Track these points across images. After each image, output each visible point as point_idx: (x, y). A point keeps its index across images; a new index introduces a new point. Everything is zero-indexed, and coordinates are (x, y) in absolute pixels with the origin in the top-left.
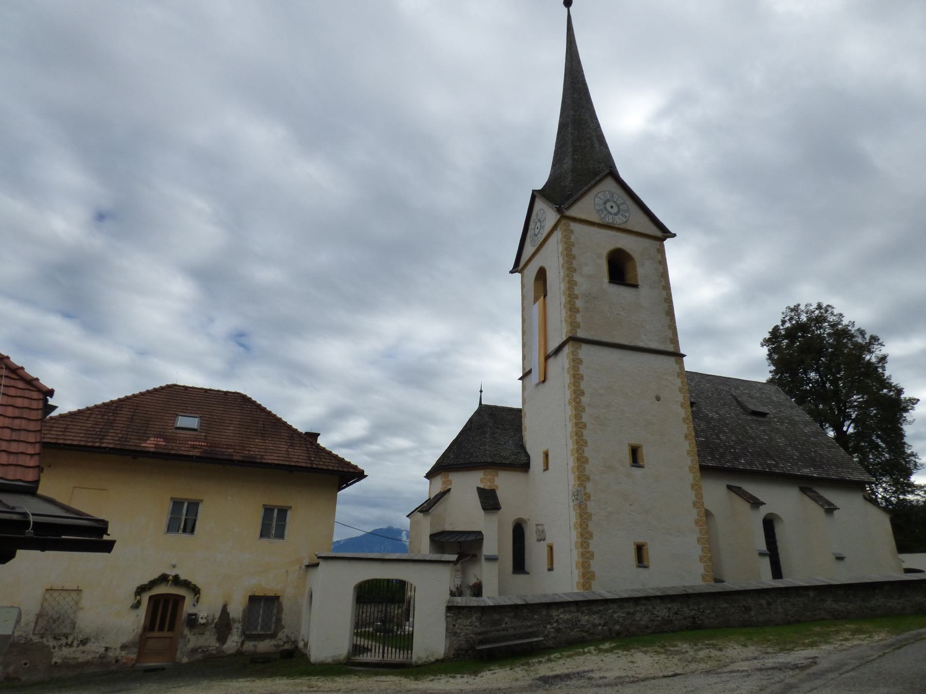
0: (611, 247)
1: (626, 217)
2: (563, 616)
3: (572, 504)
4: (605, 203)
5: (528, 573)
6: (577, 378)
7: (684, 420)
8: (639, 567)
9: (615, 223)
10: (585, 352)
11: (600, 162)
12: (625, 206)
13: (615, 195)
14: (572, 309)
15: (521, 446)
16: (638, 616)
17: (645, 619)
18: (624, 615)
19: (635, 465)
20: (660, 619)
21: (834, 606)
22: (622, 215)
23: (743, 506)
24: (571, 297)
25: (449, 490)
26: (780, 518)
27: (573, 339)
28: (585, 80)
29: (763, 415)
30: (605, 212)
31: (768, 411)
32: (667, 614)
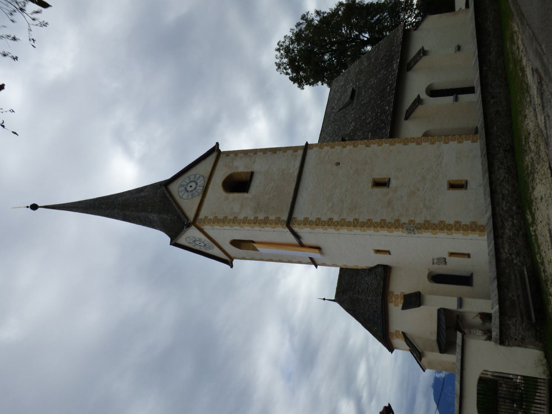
0: (221, 190)
1: (199, 177)
3: (417, 235)
4: (187, 191)
6: (318, 223)
8: (466, 188)
12: (191, 177)
13: (182, 184)
18: (504, 202)
19: (388, 184)
22: (198, 179)
23: (420, 110)
27: (289, 223)
29: (353, 92)
30: (194, 192)
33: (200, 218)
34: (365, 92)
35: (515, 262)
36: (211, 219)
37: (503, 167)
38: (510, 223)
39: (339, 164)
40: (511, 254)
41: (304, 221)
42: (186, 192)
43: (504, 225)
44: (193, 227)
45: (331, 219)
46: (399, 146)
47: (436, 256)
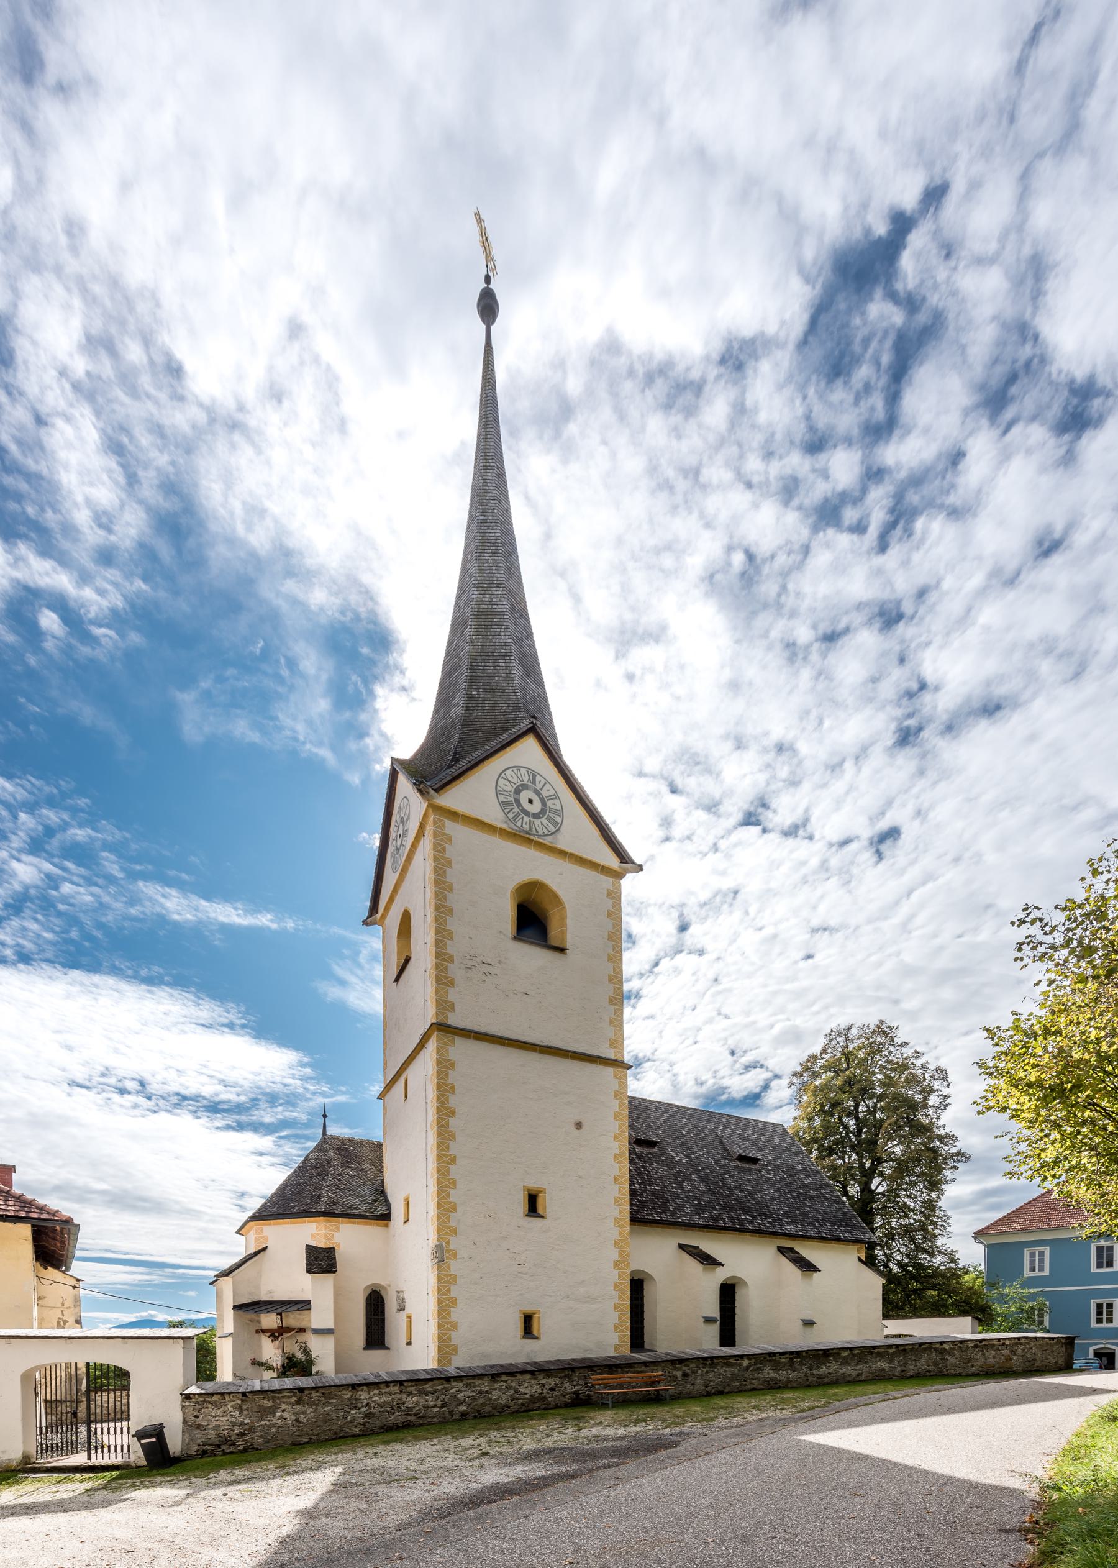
0: (526, 876)
1: (555, 824)
2: (377, 1398)
3: (430, 1264)
4: (518, 791)
5: (388, 1349)
6: (444, 1089)
7: (615, 1157)
8: (524, 1337)
9: (534, 832)
10: (461, 1049)
11: (518, 709)
12: (557, 802)
13: (538, 778)
14: (443, 980)
15: (381, 1192)
16: (495, 1395)
17: (505, 1397)
18: (473, 1394)
19: (532, 1214)
20: (528, 1396)
21: (773, 1375)
22: (549, 819)
23: (693, 1266)
24: (442, 957)
25: (266, 1248)
26: (652, 1278)
27: (441, 1027)
28: (510, 524)
29: (754, 1161)
30: (516, 810)
31: (761, 1157)
32: (539, 1391)
33: (446, 824)
34: (749, 1180)
35: (353, 1412)
36: (445, 851)
37: (545, 1391)
38: (431, 1404)
39: (578, 1129)
40: (368, 1404)
41: (447, 1060)
42: (515, 786)
43: (427, 1395)
44: (425, 805)
45: (453, 1113)
46: (613, 1232)
47: (406, 1295)
